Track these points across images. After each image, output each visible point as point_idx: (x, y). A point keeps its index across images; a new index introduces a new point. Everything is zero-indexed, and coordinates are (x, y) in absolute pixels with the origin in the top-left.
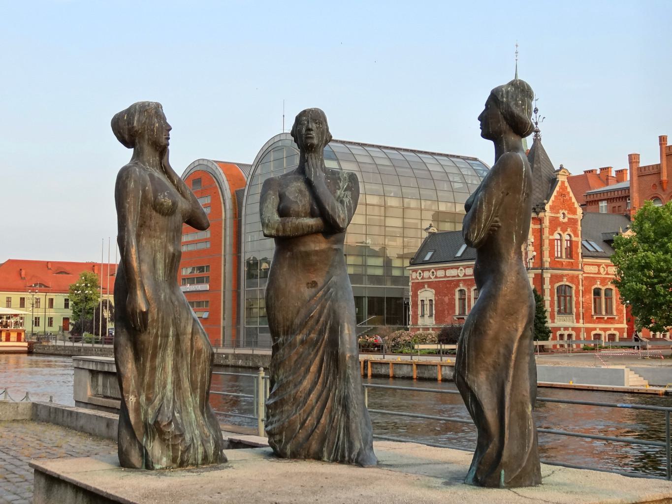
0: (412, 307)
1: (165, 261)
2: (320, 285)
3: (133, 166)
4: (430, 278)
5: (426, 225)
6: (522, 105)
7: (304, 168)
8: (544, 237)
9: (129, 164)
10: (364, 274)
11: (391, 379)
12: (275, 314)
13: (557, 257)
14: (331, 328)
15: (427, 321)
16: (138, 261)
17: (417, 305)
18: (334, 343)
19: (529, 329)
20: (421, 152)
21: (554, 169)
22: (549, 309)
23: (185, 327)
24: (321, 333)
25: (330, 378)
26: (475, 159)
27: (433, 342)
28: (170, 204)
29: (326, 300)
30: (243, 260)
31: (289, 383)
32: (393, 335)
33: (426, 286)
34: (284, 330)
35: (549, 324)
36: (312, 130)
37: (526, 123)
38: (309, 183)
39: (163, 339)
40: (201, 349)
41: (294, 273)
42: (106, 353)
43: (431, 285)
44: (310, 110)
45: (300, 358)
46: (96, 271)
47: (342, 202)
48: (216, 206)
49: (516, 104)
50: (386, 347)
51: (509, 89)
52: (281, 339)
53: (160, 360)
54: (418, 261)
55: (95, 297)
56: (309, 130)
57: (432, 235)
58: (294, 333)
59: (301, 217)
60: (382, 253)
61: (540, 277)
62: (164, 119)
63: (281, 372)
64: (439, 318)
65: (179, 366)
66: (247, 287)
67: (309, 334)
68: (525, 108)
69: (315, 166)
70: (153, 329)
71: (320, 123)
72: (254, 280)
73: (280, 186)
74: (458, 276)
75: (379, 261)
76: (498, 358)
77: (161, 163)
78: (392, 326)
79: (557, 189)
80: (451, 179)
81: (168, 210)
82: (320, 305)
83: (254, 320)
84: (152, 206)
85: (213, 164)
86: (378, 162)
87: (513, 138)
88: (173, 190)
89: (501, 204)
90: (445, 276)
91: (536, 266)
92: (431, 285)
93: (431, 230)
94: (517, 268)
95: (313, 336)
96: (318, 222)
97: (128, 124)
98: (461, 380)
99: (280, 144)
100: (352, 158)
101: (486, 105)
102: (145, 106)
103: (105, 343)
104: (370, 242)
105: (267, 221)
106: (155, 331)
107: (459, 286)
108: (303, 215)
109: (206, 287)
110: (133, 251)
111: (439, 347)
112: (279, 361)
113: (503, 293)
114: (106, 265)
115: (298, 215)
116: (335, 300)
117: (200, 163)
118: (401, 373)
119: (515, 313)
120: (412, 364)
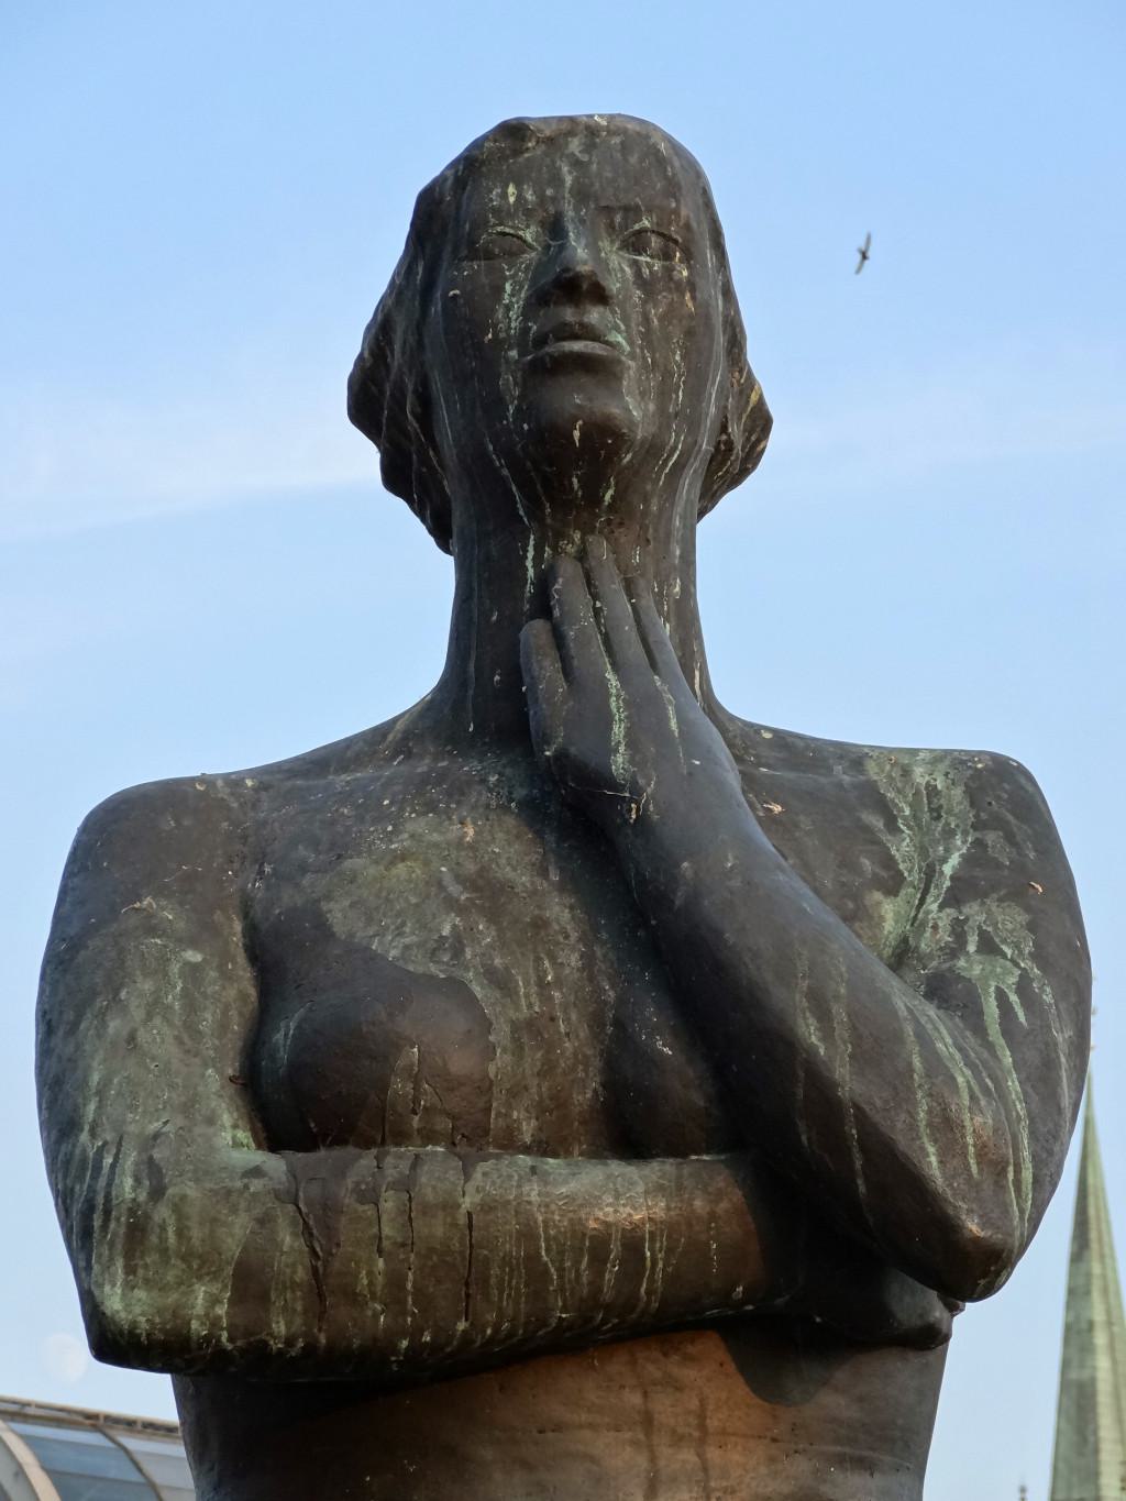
36: (600, 296)
56: (574, 288)
59: (509, 1143)
69: (633, 651)
105: (126, 1187)
108: (527, 1130)
115: (474, 1136)
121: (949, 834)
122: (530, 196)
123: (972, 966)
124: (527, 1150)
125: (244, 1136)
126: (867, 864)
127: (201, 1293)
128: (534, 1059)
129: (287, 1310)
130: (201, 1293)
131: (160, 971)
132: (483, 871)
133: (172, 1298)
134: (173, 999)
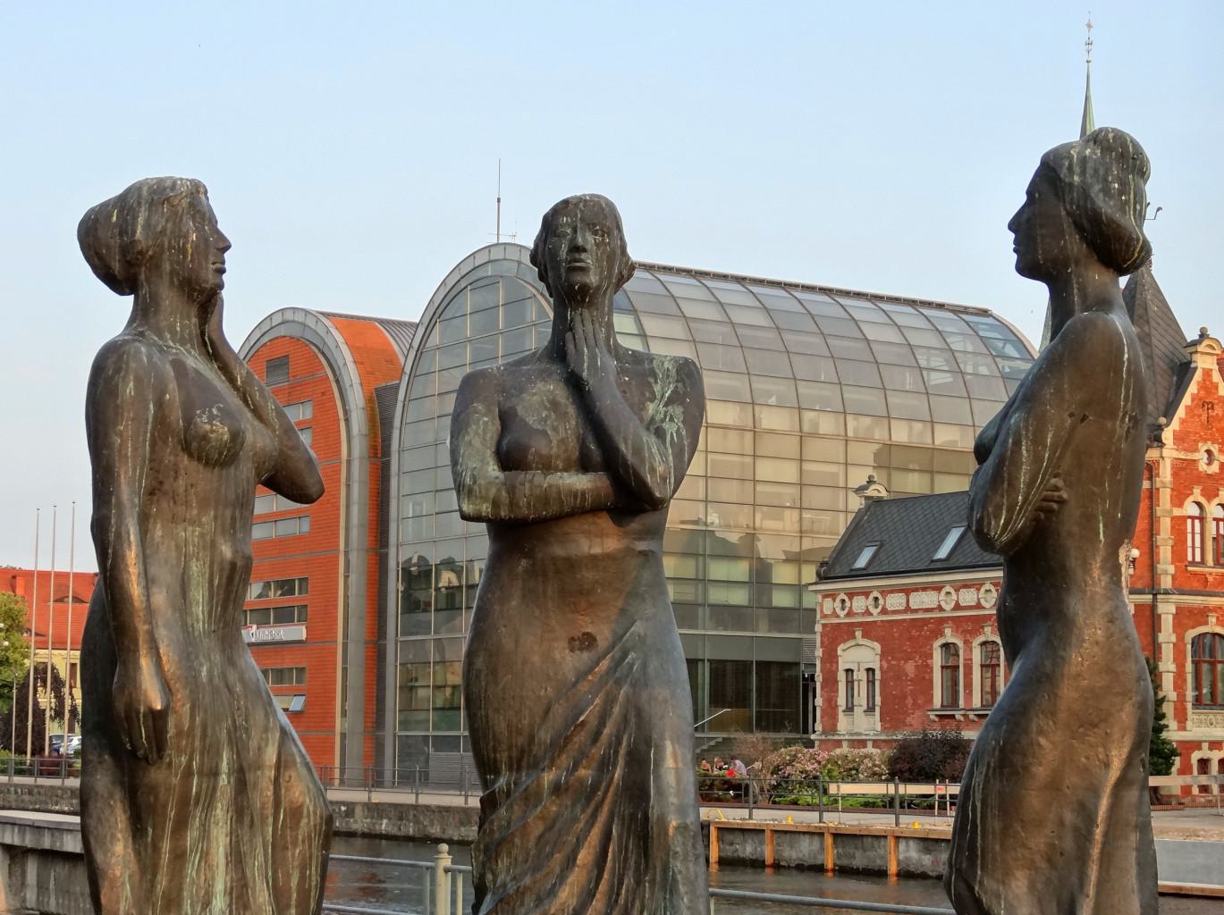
0: (822, 688)
1: (211, 581)
2: (603, 641)
3: (134, 340)
4: (868, 613)
5: (858, 477)
6: (1121, 193)
7: (564, 345)
8: (1159, 511)
9: (124, 333)
10: (700, 601)
11: (768, 871)
12: (487, 717)
13: (1193, 563)
14: (629, 754)
15: (859, 724)
16: (143, 583)
17: (836, 682)
18: (637, 791)
19: (1137, 761)
20: (847, 294)
21: (1185, 340)
22: (1172, 696)
23: (260, 749)
24: (606, 765)
25: (629, 880)
26: (984, 313)
27: (875, 777)
28: (226, 437)
29: (619, 683)
30: (392, 564)
31: (523, 894)
32: (774, 758)
33: (858, 634)
34: (510, 758)
35: (1173, 734)
36: (585, 250)
37: (1131, 239)
38: (576, 385)
39: (205, 780)
40: (301, 807)
41: (537, 612)
42: (43, 798)
43: (869, 630)
44: (581, 200)
45: (549, 828)
46: (19, 591)
47: (660, 433)
48: (326, 426)
49: (1106, 191)
50: (757, 791)
51: (1088, 152)
52: (502, 782)
53: (196, 834)
54: (838, 571)
55: (17, 656)
56: (576, 249)
57: (876, 502)
58: (535, 766)
59: (557, 470)
60: (746, 550)
61: (1148, 613)
62: (213, 221)
63: (503, 863)
64: (891, 717)
65: (245, 848)
66: (402, 634)
67: (576, 766)
68: (1127, 202)
69: (592, 342)
70: (179, 756)
71: (606, 232)
72: (421, 616)
73: (503, 392)
74: (940, 609)
75: (740, 570)
76: (1060, 838)
77: (202, 334)
78: (772, 735)
79: (1193, 388)
80: (923, 363)
81: (220, 454)
82: (601, 695)
83: (421, 716)
84: (180, 442)
85: (318, 320)
86: (738, 317)
87: (1096, 276)
88: (234, 400)
89: (1067, 443)
90: (908, 609)
91: (1139, 586)
92: (869, 630)
93: (870, 492)
94: (1106, 608)
95: (586, 773)
96: (599, 484)
97: (121, 235)
98: (965, 893)
99: (489, 271)
100: (672, 308)
101: (1030, 193)
102: (165, 189)
103: (41, 774)
104: (717, 521)
105: (468, 481)
106: (184, 759)
107: (942, 634)
108: (561, 466)
109: (298, 632)
110: (132, 556)
111: (891, 789)
112: (497, 835)
113: (1074, 670)
114: (44, 576)
115: (547, 467)
116: (640, 683)
117: (285, 317)
118: (794, 855)
119: (1105, 720)
120: (822, 834)
121: (670, 383)
122: (569, 221)
123: (666, 426)
124: (560, 471)
125: (496, 467)
126: (647, 394)
127: (484, 506)
128: (563, 448)
129: (505, 511)
130: (484, 506)
131: (478, 424)
132: (554, 399)
133: (478, 507)
134: (480, 431)
